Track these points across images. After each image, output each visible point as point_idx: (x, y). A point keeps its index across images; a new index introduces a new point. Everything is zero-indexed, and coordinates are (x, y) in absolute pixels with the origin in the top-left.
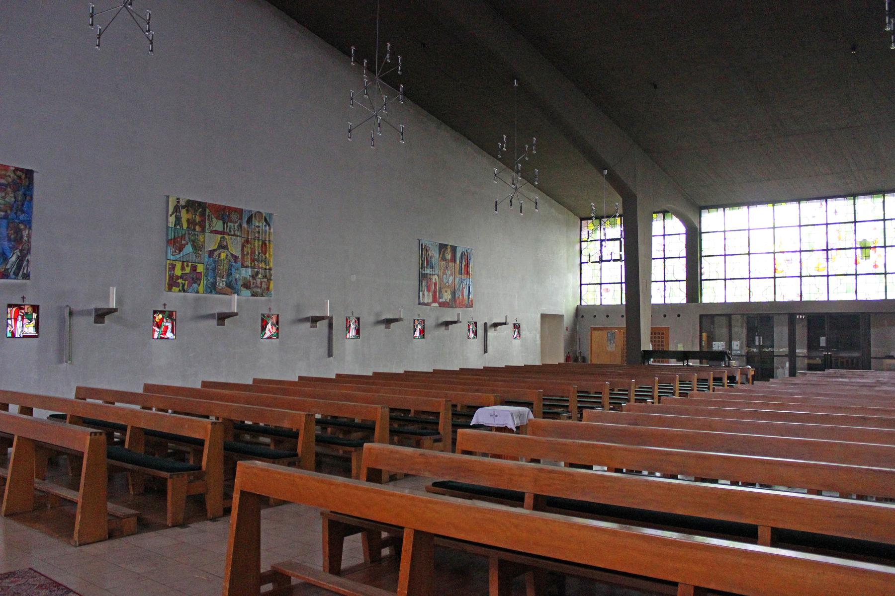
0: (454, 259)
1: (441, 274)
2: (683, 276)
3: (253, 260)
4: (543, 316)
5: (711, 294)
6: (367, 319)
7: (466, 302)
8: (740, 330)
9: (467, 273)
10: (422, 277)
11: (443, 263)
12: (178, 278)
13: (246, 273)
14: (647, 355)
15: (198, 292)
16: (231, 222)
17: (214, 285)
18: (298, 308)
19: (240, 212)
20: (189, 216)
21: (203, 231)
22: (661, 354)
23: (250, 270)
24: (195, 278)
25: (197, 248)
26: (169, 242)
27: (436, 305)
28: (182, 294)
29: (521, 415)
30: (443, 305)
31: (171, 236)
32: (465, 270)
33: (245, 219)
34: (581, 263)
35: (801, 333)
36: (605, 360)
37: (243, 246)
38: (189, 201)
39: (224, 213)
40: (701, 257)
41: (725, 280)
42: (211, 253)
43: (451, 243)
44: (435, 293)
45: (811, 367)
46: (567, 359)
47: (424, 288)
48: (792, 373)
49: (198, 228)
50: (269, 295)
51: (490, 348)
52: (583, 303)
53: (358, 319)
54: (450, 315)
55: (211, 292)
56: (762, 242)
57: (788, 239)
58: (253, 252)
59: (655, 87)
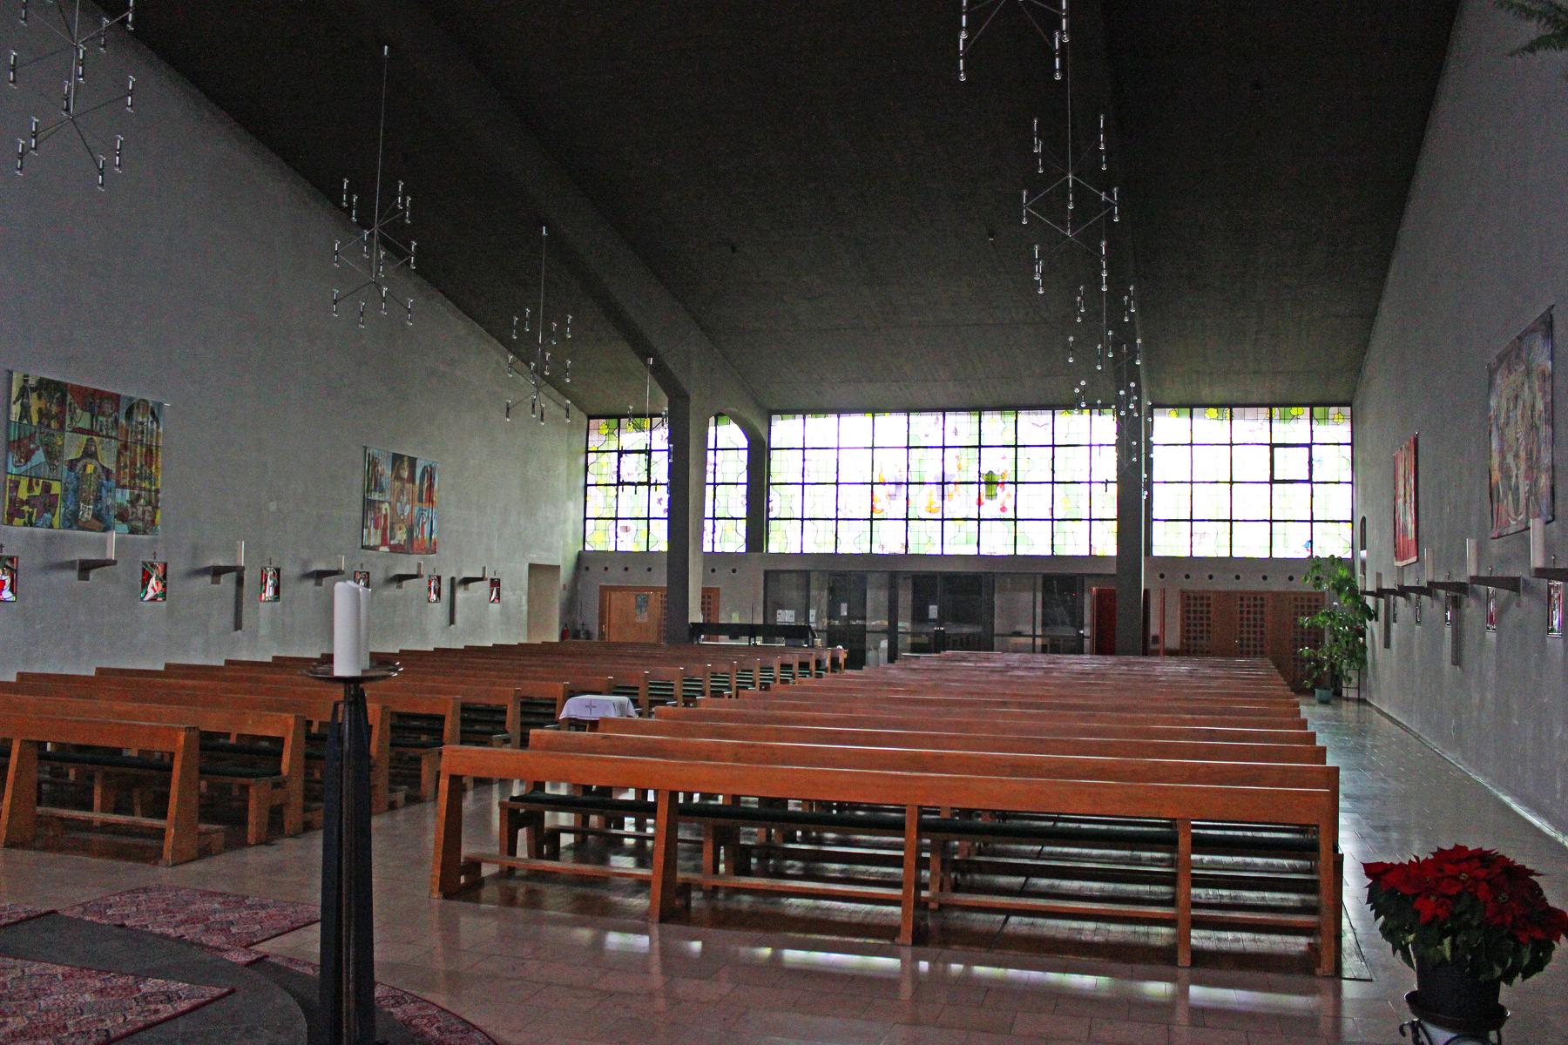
0: (412, 479)
1: (393, 500)
2: (742, 512)
3: (133, 477)
4: (532, 567)
5: (782, 540)
6: (291, 570)
7: (427, 544)
8: (820, 596)
9: (430, 500)
10: (369, 505)
11: (397, 484)
12: (23, 503)
13: (123, 497)
14: (697, 629)
15: (51, 526)
16: (103, 414)
17: (75, 514)
18: (196, 551)
19: (116, 398)
20: (42, 404)
21: (62, 428)
22: (712, 628)
23: (128, 491)
24: (48, 503)
25: (52, 455)
26: (10, 445)
27: (386, 549)
28: (28, 529)
29: (621, 706)
30: (395, 549)
31: (14, 435)
32: (427, 496)
33: (123, 412)
34: (586, 485)
35: (905, 599)
36: (630, 636)
37: (119, 454)
38: (41, 381)
39: (93, 400)
40: (769, 484)
41: (802, 519)
42: (72, 464)
43: (407, 452)
44: (384, 530)
45: (916, 648)
46: (563, 635)
47: (370, 523)
48: (893, 656)
49: (54, 424)
50: (154, 532)
51: (458, 617)
52: (588, 548)
53: (278, 570)
54: (405, 565)
55: (70, 527)
56: (855, 467)
57: (891, 465)
58: (133, 463)
59: (734, 250)
